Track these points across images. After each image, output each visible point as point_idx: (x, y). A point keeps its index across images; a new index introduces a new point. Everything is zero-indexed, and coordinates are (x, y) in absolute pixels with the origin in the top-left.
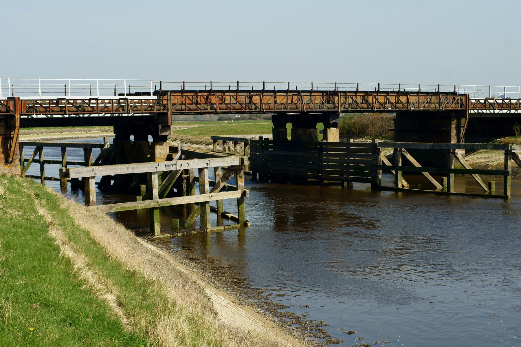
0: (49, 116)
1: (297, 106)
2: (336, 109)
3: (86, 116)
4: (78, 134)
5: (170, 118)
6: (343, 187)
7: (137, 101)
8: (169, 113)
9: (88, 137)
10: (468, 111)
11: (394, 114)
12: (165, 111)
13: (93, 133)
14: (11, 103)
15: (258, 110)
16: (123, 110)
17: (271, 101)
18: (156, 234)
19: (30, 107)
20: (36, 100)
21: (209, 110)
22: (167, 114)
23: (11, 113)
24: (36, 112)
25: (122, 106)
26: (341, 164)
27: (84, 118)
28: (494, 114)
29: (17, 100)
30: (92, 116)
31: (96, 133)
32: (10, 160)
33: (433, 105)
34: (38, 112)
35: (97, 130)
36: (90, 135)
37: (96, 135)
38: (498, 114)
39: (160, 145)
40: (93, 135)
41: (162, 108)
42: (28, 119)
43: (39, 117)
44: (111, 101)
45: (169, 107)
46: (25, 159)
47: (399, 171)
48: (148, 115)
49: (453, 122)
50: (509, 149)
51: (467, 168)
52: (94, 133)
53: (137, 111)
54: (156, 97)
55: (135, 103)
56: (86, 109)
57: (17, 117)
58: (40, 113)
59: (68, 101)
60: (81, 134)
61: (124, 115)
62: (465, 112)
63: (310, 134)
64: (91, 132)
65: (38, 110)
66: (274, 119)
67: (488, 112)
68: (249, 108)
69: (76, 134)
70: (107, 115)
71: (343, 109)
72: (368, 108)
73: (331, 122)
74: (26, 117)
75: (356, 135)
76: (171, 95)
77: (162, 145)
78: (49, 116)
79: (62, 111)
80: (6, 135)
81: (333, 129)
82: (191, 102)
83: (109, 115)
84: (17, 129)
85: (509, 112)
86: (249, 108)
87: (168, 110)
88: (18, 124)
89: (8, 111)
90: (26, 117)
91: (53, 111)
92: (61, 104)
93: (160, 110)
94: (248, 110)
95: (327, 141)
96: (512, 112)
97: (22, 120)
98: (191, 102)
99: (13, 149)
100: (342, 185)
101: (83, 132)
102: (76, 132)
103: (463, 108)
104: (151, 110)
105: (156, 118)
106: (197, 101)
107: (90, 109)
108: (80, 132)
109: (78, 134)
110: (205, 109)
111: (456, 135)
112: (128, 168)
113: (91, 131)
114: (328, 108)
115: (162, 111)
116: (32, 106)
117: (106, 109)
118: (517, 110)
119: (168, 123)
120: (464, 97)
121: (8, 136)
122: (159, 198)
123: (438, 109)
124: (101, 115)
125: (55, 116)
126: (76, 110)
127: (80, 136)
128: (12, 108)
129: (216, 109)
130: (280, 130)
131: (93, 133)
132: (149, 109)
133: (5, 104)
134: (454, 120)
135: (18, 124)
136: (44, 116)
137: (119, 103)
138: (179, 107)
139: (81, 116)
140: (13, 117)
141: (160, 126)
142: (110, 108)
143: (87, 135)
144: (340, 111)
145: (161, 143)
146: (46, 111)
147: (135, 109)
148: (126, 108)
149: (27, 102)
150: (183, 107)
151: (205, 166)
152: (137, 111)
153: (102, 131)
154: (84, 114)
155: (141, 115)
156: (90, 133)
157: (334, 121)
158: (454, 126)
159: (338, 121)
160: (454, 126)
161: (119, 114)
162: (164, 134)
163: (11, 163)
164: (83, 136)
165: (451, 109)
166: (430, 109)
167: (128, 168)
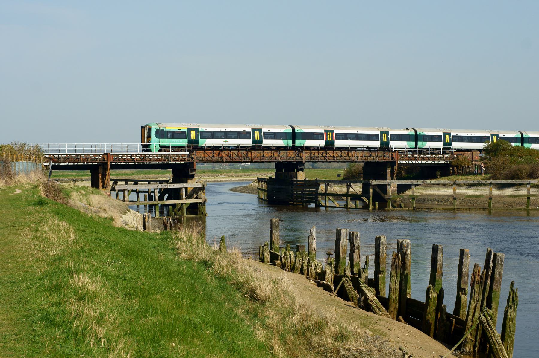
0: (127, 163)
1: (276, 159)
2: (302, 160)
3: (148, 163)
4: (207, 178)
5: (195, 165)
6: (303, 206)
7: (93, 156)
8: (195, 162)
9: (215, 181)
10: (397, 162)
11: (362, 164)
12: (192, 161)
13: (220, 178)
14: (106, 156)
15: (250, 161)
16: (168, 160)
17: (285, 155)
18: (157, 216)
19: (115, 158)
20: (119, 155)
21: (220, 161)
22: (193, 162)
23: (106, 162)
24: (119, 161)
25: (168, 158)
26: (302, 193)
27: (146, 164)
28: (421, 163)
29: (109, 155)
30: (151, 163)
31: (223, 178)
32: (105, 186)
33: (372, 158)
34: (119, 161)
35: (224, 175)
36: (217, 179)
37: (223, 179)
38: (425, 163)
39: (190, 180)
40: (220, 179)
41: (191, 159)
42: (115, 164)
43: (121, 163)
44: (161, 155)
45: (304, 158)
46: (340, 230)
47: (357, 201)
48: (184, 163)
49: (388, 169)
50: (370, 183)
51: (359, 194)
52: (221, 178)
53: (176, 161)
54: (188, 153)
55: (175, 156)
56: (147, 159)
57: (109, 163)
58: (122, 161)
59: (136, 155)
60: (209, 178)
61: (169, 163)
62: (395, 162)
63: (291, 175)
64: (219, 177)
65: (120, 160)
66: (276, 166)
67: (417, 162)
68: (244, 159)
69: (204, 178)
70: (159, 163)
71: (306, 160)
72: (324, 160)
73: (299, 168)
74: (114, 163)
75: (357, 177)
76: (196, 152)
77: (192, 180)
78: (127, 163)
79: (133, 160)
80: (103, 173)
81: (301, 172)
82: (330, 156)
83: (161, 163)
84: (108, 170)
85: (433, 162)
86: (244, 159)
87: (194, 160)
88: (109, 167)
89: (104, 161)
90: (114, 163)
91: (128, 161)
92: (133, 157)
93: (189, 160)
94: (244, 161)
95: (297, 178)
96: (436, 162)
97: (111, 165)
98: (330, 156)
99: (106, 180)
100: (302, 205)
101: (211, 177)
102: (204, 177)
103: (394, 160)
104: (185, 160)
105: (188, 164)
106: (341, 155)
107: (149, 160)
108: (208, 177)
109: (207, 178)
110: (217, 160)
111: (390, 176)
112: (143, 186)
113: (219, 176)
114: (297, 160)
115: (191, 161)
116: (117, 158)
117: (175, 159)
118: (440, 161)
119: (194, 168)
120: (394, 153)
121: (104, 173)
122: (159, 200)
123: (375, 160)
124: (156, 163)
125: (130, 163)
126: (141, 160)
127: (208, 180)
128: (106, 159)
129: (327, 160)
130: (279, 172)
131: (220, 178)
132: (183, 159)
133: (103, 157)
134: (389, 167)
135: (109, 167)
136: (124, 163)
137: (166, 156)
138: (201, 158)
139: (145, 163)
140: (107, 163)
141: (190, 169)
142: (161, 159)
143: (214, 180)
144: (304, 161)
145: (191, 179)
146: (124, 160)
147: (175, 160)
148: (169, 159)
149: (114, 156)
150: (204, 158)
151: (183, 187)
152: (176, 161)
153: (229, 176)
154: (146, 162)
155: (179, 163)
156: (218, 178)
157: (301, 167)
158: (389, 171)
159: (303, 168)
160: (389, 171)
161: (167, 162)
162: (192, 173)
163: (105, 188)
164: (211, 180)
165: (384, 160)
166: (369, 160)
167: (143, 186)
